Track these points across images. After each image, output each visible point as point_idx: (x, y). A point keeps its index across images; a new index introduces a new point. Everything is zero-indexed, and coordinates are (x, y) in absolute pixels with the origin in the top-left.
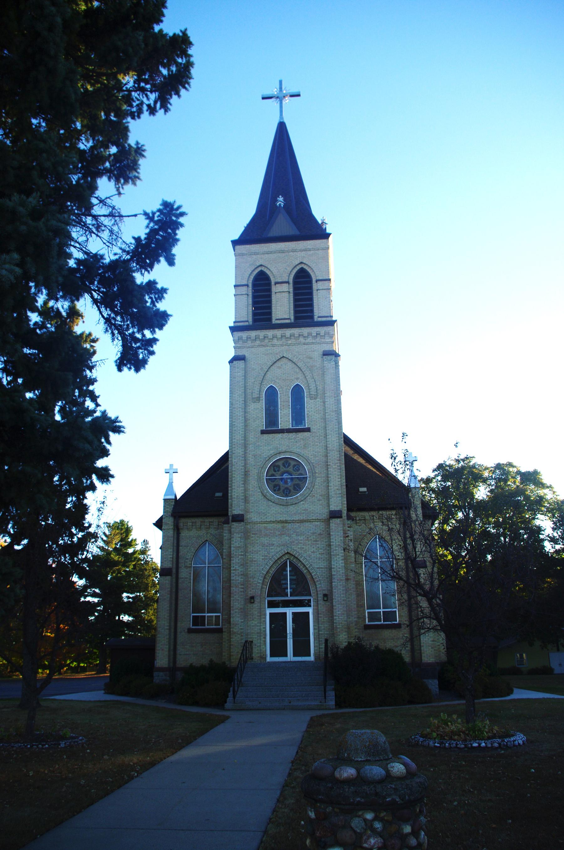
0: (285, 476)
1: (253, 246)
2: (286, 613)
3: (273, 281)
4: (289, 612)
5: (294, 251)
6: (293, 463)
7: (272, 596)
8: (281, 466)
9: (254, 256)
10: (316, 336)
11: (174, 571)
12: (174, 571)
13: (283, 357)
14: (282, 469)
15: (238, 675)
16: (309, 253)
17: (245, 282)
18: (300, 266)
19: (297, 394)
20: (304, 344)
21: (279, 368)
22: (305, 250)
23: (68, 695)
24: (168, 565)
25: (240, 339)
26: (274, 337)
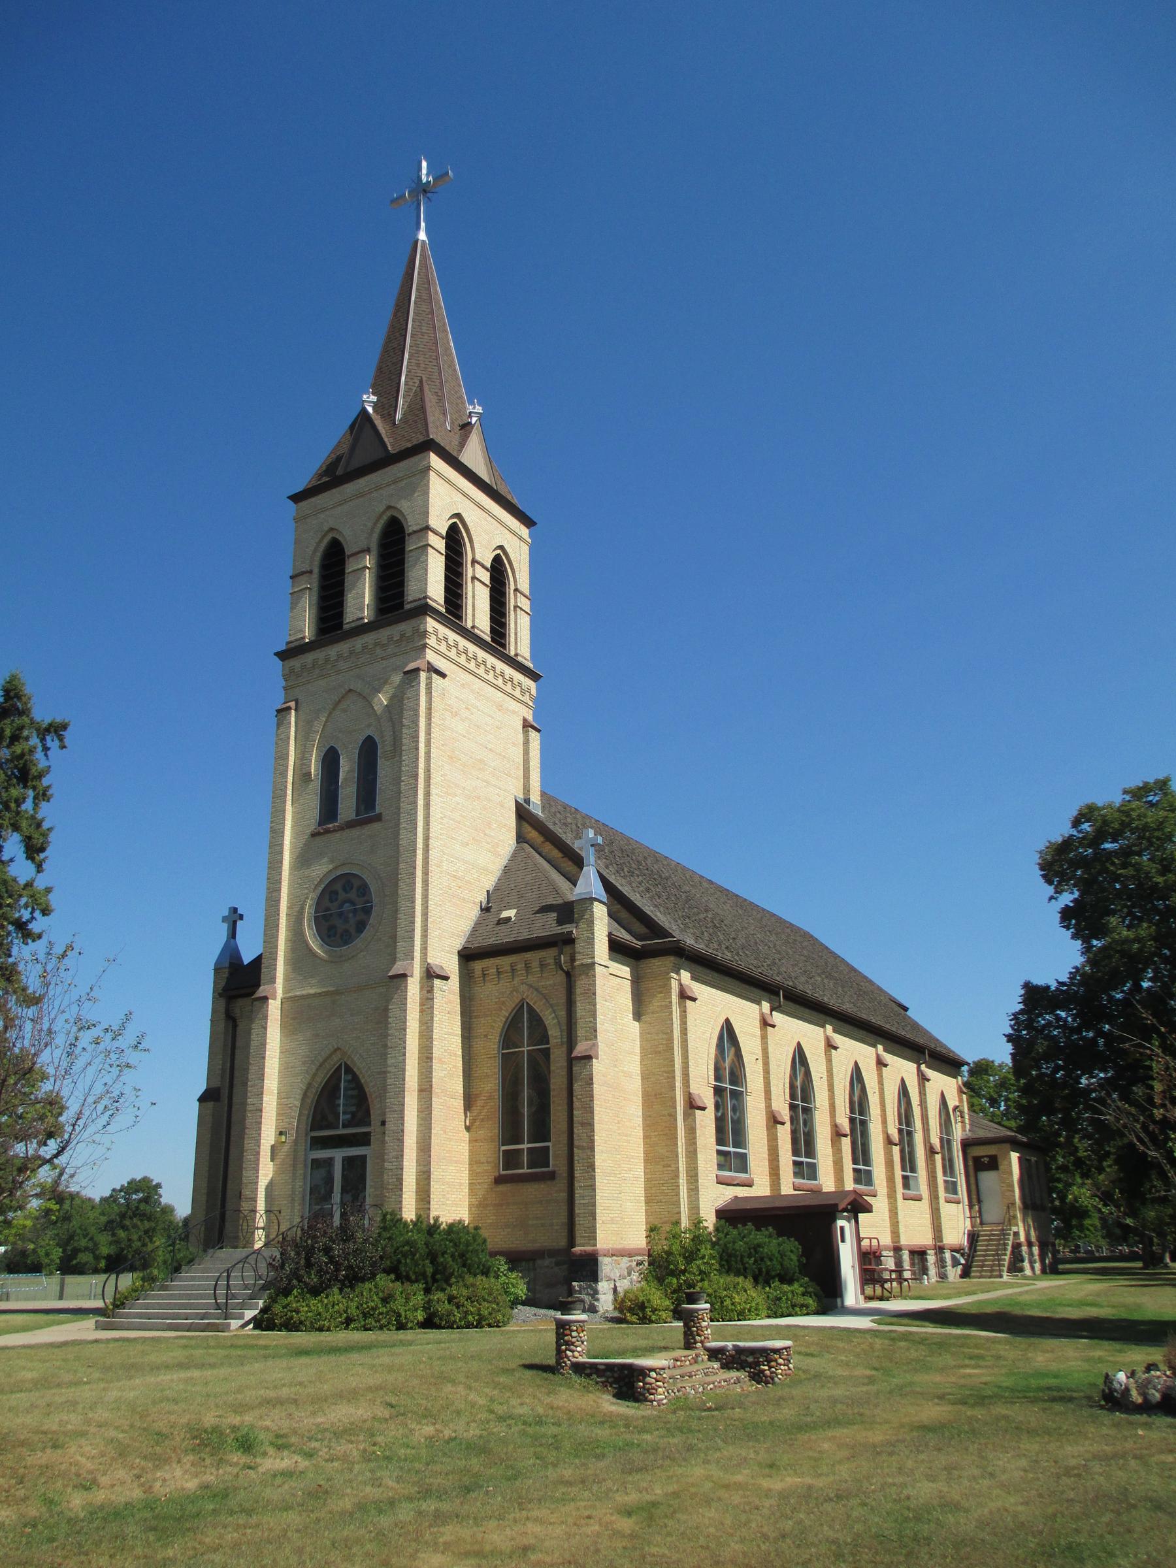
0: (347, 907)
1: (320, 496)
2: (365, 1156)
3: (347, 552)
4: (338, 1155)
5: (379, 488)
6: (338, 887)
7: (321, 1128)
8: (340, 891)
9: (322, 516)
10: (401, 640)
11: (225, 1093)
12: (225, 1093)
13: (350, 690)
14: (342, 896)
15: (1021, 1293)
16: (403, 484)
17: (306, 567)
18: (389, 514)
19: (369, 752)
20: (383, 658)
21: (345, 711)
22: (395, 482)
23: (7, 1336)
24: (216, 1083)
25: (292, 671)
26: (340, 656)
